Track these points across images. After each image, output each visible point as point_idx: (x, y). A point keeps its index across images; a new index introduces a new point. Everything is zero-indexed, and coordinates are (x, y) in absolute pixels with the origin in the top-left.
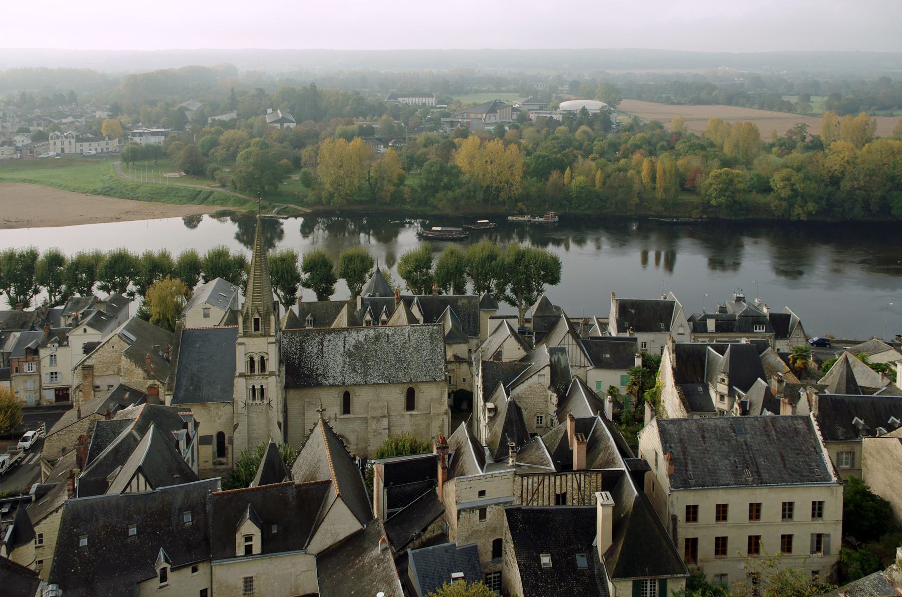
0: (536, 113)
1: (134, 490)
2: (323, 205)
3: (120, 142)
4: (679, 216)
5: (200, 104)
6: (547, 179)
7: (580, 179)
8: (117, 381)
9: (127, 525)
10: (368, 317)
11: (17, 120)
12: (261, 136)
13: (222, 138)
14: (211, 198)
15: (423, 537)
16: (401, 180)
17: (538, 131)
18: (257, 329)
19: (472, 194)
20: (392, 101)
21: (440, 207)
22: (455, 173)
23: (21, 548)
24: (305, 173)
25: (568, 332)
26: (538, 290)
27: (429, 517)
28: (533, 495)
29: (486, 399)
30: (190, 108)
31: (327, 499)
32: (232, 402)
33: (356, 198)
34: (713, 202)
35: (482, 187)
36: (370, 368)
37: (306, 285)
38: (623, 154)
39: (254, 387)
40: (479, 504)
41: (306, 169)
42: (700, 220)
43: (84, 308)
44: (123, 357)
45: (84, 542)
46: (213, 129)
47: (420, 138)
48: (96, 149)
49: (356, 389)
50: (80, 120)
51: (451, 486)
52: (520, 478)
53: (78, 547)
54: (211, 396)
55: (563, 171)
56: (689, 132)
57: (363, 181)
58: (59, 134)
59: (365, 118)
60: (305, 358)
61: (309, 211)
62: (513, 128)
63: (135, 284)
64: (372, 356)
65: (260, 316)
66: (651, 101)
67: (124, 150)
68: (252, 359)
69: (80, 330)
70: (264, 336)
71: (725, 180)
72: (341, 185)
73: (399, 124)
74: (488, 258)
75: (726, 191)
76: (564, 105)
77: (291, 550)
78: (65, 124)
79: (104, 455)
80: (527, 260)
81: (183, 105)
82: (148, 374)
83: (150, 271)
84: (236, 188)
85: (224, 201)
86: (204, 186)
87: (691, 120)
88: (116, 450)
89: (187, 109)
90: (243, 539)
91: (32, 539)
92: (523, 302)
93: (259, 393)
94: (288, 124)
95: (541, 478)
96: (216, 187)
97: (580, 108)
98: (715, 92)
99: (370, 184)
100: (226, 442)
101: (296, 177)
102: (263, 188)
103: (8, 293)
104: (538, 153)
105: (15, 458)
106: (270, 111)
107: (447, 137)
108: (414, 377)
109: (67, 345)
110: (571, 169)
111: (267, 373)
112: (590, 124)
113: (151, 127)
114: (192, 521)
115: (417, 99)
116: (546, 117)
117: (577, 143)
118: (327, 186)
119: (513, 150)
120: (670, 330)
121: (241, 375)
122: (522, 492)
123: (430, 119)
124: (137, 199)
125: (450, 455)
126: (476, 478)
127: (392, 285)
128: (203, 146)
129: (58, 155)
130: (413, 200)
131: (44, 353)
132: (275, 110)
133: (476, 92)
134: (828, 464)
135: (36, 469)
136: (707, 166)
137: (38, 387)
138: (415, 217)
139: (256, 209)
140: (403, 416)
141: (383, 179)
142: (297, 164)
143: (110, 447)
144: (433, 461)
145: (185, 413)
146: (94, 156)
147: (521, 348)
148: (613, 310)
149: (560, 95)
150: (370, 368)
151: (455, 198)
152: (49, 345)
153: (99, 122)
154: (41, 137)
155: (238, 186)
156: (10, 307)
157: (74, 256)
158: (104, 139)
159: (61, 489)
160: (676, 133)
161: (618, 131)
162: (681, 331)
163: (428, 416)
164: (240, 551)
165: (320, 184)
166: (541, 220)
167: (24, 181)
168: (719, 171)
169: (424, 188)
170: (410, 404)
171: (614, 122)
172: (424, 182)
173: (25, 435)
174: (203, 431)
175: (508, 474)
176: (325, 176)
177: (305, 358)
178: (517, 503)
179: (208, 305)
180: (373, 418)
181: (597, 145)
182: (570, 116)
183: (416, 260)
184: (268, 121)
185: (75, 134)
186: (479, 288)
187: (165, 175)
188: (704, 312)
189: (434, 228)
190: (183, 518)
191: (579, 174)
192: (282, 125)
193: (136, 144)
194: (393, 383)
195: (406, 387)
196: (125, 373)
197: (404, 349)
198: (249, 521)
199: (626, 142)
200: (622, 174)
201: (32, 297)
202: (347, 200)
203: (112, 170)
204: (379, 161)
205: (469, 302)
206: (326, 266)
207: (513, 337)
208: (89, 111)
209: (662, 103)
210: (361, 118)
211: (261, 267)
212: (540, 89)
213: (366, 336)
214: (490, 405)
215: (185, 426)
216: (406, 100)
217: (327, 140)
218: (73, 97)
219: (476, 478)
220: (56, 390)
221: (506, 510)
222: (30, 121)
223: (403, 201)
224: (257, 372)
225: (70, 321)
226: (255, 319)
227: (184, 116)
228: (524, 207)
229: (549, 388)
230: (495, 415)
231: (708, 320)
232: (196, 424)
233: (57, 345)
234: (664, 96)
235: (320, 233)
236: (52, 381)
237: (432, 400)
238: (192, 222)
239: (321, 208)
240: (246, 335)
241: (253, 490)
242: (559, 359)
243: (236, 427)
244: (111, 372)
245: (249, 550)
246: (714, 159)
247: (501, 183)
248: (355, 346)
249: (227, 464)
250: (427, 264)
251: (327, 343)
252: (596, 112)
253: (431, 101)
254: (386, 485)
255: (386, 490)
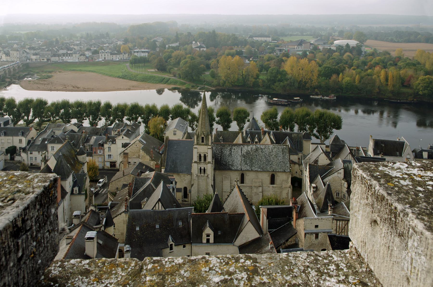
0: (322, 46)
1: (157, 209)
2: (221, 86)
3: (128, 55)
4: (400, 99)
5: (162, 39)
6: (330, 78)
7: (347, 79)
8: (138, 161)
9: (155, 224)
10: (249, 140)
11: (86, 45)
12: (190, 54)
13: (173, 55)
14: (169, 82)
15: (286, 244)
16: (258, 76)
17: (324, 55)
18: (203, 142)
19: (292, 84)
20: (250, 39)
21: (276, 90)
22: (284, 74)
23: (109, 228)
24: (212, 72)
25: (350, 153)
26: (330, 132)
27: (289, 235)
28: (342, 230)
29: (311, 182)
30: (158, 40)
31: (243, 222)
32: (191, 174)
33: (236, 84)
34: (421, 93)
35: (297, 81)
36: (253, 163)
37: (218, 123)
38: (369, 67)
39: (201, 168)
40: (315, 231)
41: (213, 69)
42: (413, 102)
43: (122, 127)
44: (141, 150)
45: (138, 229)
46: (169, 50)
47: (266, 57)
48: (119, 58)
49: (247, 172)
50: (111, 45)
51: (301, 222)
52: (336, 221)
53: (135, 231)
54: (181, 171)
55: (338, 74)
56: (405, 57)
57: (239, 76)
58: (103, 51)
59: (238, 47)
60: (223, 156)
61: (214, 89)
62: (311, 53)
63: (142, 118)
64: (255, 158)
65: (204, 135)
66: (383, 40)
67: (131, 58)
68: (200, 155)
69: (120, 137)
70: (206, 145)
71: (428, 82)
72: (229, 78)
73: (254, 50)
74: (306, 115)
75: (428, 87)
76: (336, 42)
77: (227, 243)
78: (105, 47)
79: (139, 192)
80: (325, 117)
81: (155, 39)
82: (152, 159)
83: (148, 113)
84: (180, 77)
85: (175, 83)
86: (166, 76)
87: (405, 50)
88: (144, 190)
89: (157, 41)
90: (206, 236)
91: (112, 225)
92: (323, 137)
93: (203, 171)
94: (203, 49)
95: (346, 222)
96: (171, 76)
97: (346, 44)
98: (419, 36)
99: (243, 77)
100: (188, 192)
101: (208, 73)
102: (193, 78)
103: (89, 119)
104: (325, 65)
105: (97, 190)
106: (194, 42)
107: (278, 57)
108: (275, 169)
109: (115, 143)
110: (342, 74)
111: (207, 162)
112: (351, 52)
113: (141, 49)
114: (182, 225)
115: (262, 38)
116: (327, 48)
117: (345, 61)
118: (223, 78)
119: (313, 63)
120: (402, 156)
121: (195, 162)
122: (337, 227)
123: (269, 48)
124: (137, 81)
125: (298, 207)
126: (314, 219)
127: (259, 125)
128: (165, 58)
129: (103, 60)
130: (263, 86)
131: (106, 146)
132: (196, 42)
133: (291, 35)
134: (85, 261)
135: (105, 196)
136: (417, 74)
137: (103, 161)
138: (264, 93)
139: (190, 87)
140: (269, 187)
141: (249, 76)
142: (208, 67)
143: (141, 189)
144: (290, 210)
145: (171, 177)
146: (118, 61)
147: (328, 159)
148: (371, 144)
149: (334, 37)
150: (253, 163)
151: (284, 86)
152: (108, 143)
153: (120, 46)
154: (96, 52)
155: (182, 76)
156: (90, 126)
157: (116, 105)
158: (122, 54)
159: (121, 205)
160: (398, 57)
161: (366, 56)
162: (408, 157)
163: (281, 188)
164: (204, 241)
165: (219, 76)
166: (327, 98)
167: (90, 71)
168: (424, 77)
169: (269, 80)
170: (273, 182)
171: (363, 51)
172: (269, 77)
173: (99, 181)
174: (178, 186)
175: (330, 219)
176: (222, 73)
177: (223, 156)
178: (334, 233)
179: (176, 130)
180: (255, 186)
181: (355, 62)
182: (340, 48)
183: (271, 114)
184: (193, 47)
185: (110, 51)
186: (300, 129)
187: (149, 70)
188: (421, 148)
189: (274, 99)
190: (178, 223)
191: (347, 77)
192: (200, 49)
193: (136, 56)
194: (265, 171)
195: (271, 173)
196: (142, 157)
197: (270, 155)
198: (209, 228)
199: (371, 61)
200: (369, 77)
201: (98, 121)
202: (232, 84)
203: (126, 68)
204: (247, 67)
205: (298, 136)
206: (227, 115)
207: (324, 154)
208: (114, 41)
209: (388, 42)
210: (236, 47)
211: (205, 114)
212: (323, 34)
213: (251, 148)
214: (314, 185)
215: (172, 183)
216: (257, 38)
217: (223, 57)
218: (107, 34)
219: (314, 219)
220: (111, 162)
221: (329, 236)
222: (91, 45)
223: (259, 86)
224: (202, 161)
225: (116, 133)
226: (202, 137)
227: (155, 44)
228: (318, 91)
229: (343, 179)
230: (316, 190)
231: (423, 152)
232: (176, 183)
233: (111, 143)
234: (390, 38)
235: (219, 99)
236: (109, 158)
237: (283, 180)
238: (160, 92)
239: (220, 88)
240: (198, 144)
241: (207, 214)
242: (348, 166)
243: (192, 185)
244: (135, 157)
245: (208, 241)
246: (421, 71)
247: (307, 79)
248: (246, 153)
249: (188, 202)
250: (275, 116)
251: (233, 150)
252: (354, 46)
253: (269, 39)
254: (268, 218)
255: (268, 220)
